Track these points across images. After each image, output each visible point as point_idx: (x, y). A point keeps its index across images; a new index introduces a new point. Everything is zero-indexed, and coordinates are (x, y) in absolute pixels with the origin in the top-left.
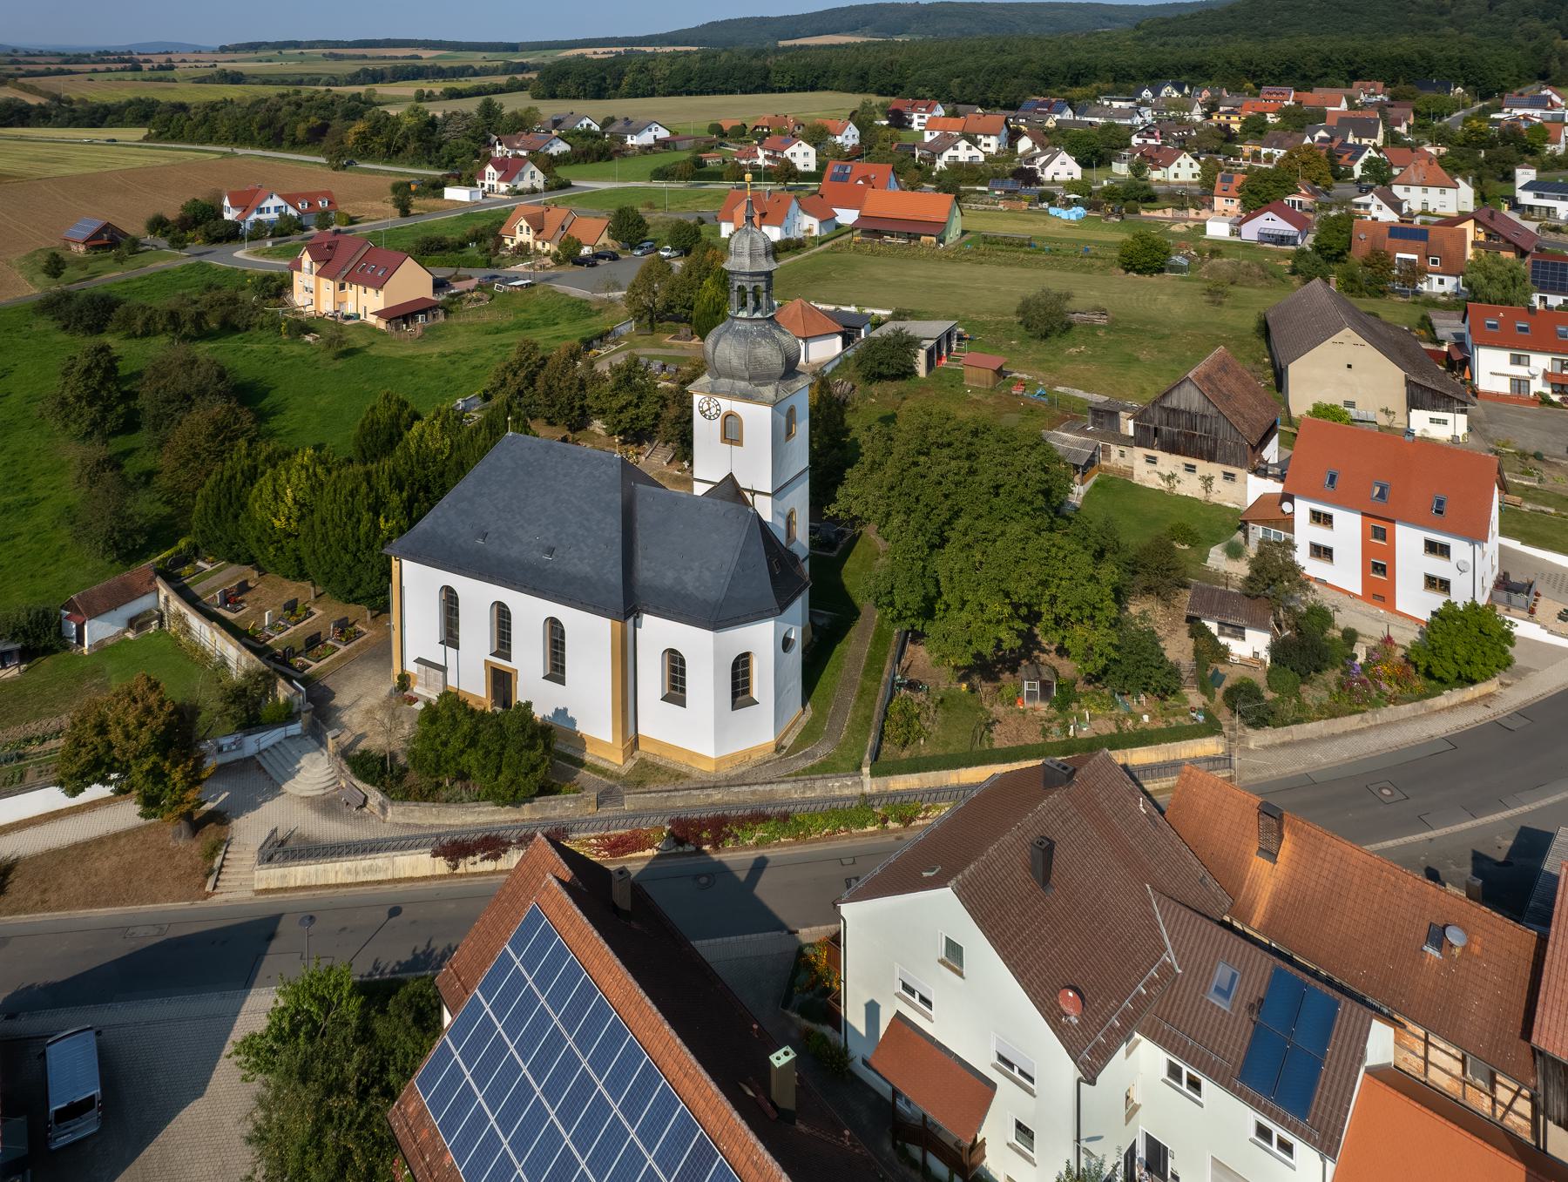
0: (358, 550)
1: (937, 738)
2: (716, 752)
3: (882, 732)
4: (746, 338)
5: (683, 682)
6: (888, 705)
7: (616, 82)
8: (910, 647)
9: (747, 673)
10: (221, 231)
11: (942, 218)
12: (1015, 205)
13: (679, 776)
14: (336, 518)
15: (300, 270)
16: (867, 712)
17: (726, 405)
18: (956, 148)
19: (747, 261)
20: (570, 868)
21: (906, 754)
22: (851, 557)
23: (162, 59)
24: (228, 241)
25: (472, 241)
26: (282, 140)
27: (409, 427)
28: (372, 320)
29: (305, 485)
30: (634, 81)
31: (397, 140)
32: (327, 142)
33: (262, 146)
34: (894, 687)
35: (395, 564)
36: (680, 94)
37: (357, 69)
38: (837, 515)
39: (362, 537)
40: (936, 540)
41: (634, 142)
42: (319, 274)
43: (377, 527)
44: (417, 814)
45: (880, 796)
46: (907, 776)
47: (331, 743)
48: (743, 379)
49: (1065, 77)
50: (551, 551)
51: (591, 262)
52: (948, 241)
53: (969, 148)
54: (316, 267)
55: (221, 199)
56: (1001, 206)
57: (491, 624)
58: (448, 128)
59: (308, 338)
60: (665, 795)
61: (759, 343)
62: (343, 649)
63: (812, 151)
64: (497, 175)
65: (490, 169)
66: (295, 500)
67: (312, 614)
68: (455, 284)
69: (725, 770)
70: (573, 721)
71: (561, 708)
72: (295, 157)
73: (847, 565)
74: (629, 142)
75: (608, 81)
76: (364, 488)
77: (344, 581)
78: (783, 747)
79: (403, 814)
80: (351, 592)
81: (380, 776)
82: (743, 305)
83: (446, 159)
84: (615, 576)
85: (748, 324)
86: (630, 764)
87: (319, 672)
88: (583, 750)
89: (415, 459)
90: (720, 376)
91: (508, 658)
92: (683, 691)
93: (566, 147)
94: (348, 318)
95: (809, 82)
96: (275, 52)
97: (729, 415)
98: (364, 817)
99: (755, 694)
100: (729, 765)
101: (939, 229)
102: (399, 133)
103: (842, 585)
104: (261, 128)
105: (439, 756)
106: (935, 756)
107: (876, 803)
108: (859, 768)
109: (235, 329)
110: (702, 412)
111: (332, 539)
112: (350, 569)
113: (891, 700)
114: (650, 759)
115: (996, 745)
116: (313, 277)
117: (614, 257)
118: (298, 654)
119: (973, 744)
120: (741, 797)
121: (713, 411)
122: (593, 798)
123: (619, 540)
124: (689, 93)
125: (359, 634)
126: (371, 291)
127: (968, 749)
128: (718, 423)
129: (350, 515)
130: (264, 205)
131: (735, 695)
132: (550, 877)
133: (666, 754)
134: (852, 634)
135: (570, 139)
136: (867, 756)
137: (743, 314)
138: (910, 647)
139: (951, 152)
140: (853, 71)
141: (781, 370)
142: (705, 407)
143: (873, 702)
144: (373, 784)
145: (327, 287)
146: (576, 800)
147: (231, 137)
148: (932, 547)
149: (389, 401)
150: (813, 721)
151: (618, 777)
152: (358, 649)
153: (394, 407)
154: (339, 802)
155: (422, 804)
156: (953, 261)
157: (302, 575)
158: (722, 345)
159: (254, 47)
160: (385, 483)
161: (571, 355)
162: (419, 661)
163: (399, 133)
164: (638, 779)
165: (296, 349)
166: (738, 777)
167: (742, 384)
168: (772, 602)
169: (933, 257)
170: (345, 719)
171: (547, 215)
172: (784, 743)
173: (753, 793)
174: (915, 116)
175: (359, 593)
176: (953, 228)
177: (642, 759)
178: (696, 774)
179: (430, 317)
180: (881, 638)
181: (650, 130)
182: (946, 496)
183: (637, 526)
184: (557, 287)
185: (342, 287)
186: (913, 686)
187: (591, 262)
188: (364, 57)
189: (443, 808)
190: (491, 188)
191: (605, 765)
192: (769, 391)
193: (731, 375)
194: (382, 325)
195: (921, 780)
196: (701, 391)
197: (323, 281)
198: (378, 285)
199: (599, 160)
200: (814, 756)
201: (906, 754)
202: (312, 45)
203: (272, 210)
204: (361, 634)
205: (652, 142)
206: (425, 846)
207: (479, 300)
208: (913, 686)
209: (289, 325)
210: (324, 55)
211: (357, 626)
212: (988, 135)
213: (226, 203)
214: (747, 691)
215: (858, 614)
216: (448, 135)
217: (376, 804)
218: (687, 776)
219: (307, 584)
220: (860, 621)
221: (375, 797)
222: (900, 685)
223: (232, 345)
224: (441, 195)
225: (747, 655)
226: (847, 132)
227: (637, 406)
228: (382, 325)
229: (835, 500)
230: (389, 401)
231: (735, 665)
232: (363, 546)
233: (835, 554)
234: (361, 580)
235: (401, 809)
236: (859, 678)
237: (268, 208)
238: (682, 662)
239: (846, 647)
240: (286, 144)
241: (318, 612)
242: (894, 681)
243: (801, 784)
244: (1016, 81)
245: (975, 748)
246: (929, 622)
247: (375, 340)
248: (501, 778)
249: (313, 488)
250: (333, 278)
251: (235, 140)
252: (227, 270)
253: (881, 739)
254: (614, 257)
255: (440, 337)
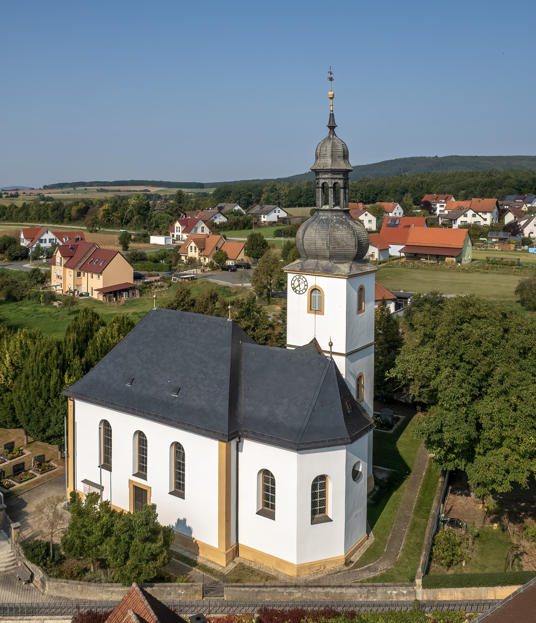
0: (49, 398)
1: (476, 562)
2: (299, 557)
3: (431, 554)
4: (328, 224)
5: (273, 499)
6: (435, 534)
7: (258, 198)
8: (450, 496)
9: (323, 494)
10: (18, 253)
11: (460, 245)
12: (506, 246)
13: (268, 577)
14: (35, 372)
15: (55, 265)
16: (418, 540)
17: (312, 280)
18: (466, 216)
19: (329, 161)
20: (156, 613)
21: (451, 572)
22: (404, 434)
23: (14, 193)
24: (22, 260)
25: (162, 259)
26: (64, 218)
27: (97, 330)
28: (96, 296)
29: (19, 352)
30: (268, 197)
31: (127, 215)
32: (89, 218)
33: (53, 222)
34: (439, 524)
35: (70, 403)
36: (295, 206)
37: (113, 196)
38: (396, 377)
39: (52, 389)
40: (476, 392)
41: (265, 220)
42: (65, 266)
43: (63, 382)
44: (67, 589)
45: (431, 604)
46: (452, 590)
47: (13, 533)
48: (324, 258)
49: (531, 188)
50: (178, 391)
51: (233, 269)
52: (463, 262)
53: (474, 216)
54: (64, 261)
55: (19, 235)
56: (496, 248)
57: (134, 450)
58: (156, 208)
59: (56, 304)
60: (256, 590)
61: (338, 228)
62: (39, 476)
63: (374, 219)
64: (182, 229)
65: (177, 224)
66: (12, 364)
67: (23, 454)
68: (148, 278)
69: (305, 576)
70: (190, 530)
71: (181, 518)
72: (70, 227)
73: (401, 439)
74: (263, 219)
75: (253, 197)
76: (55, 352)
77: (38, 421)
78: (352, 562)
79: (56, 588)
80: (44, 431)
81: (43, 558)
82: (326, 203)
83: (154, 225)
84: (223, 406)
85: (329, 214)
86: (232, 566)
87: (20, 490)
88: (197, 554)
89: (99, 350)
90: (307, 258)
91: (145, 477)
92: (273, 507)
93: (224, 220)
94: (82, 295)
95: (371, 197)
96: (72, 189)
97: (315, 289)
98: (30, 590)
99: (330, 513)
100: (307, 572)
101: (458, 253)
102: (128, 210)
103: (397, 452)
104: (53, 211)
105: (83, 543)
106: (475, 575)
107: (427, 609)
108: (413, 580)
109: (15, 300)
110: (294, 288)
111: (31, 387)
112: (43, 411)
113: (437, 531)
114: (247, 564)
115: (525, 569)
116: (62, 268)
117: (248, 267)
118: (8, 477)
119: (506, 569)
120: (317, 597)
121: (302, 286)
122: (200, 588)
123: (227, 381)
124: (300, 205)
125: (51, 468)
126: (95, 276)
127: (503, 571)
128: (305, 297)
129: (44, 370)
130: (43, 238)
131: (314, 512)
132: (130, 613)
133: (259, 560)
134: (405, 485)
135: (227, 216)
136: (420, 570)
137: (327, 207)
138: (450, 496)
139: (462, 218)
140: (399, 189)
141: (353, 250)
142: (296, 284)
143: (423, 533)
144: (38, 564)
145: (70, 273)
146: (186, 588)
147: (37, 218)
148: (474, 398)
149: (87, 313)
150: (375, 545)
151: (221, 575)
152: (49, 476)
153: (90, 317)
154: (15, 577)
155: (71, 581)
156: (467, 271)
157: (16, 423)
158: (309, 230)
159: (61, 186)
160: (70, 350)
161: (211, 297)
162: (86, 482)
163: (128, 210)
164: (237, 578)
165: (47, 309)
166: (314, 581)
167: (324, 263)
168: (346, 435)
169: (453, 269)
170: (30, 521)
171: (207, 240)
172: (352, 558)
173: (327, 594)
174: (438, 205)
175: (49, 432)
176: (467, 254)
177: (241, 564)
178: (281, 577)
179: (131, 294)
180: (428, 488)
181: (275, 212)
182: (485, 354)
183: (242, 373)
184: (211, 280)
185: (79, 275)
186: (454, 523)
187: (233, 269)
188: (119, 191)
189: (85, 585)
190: (178, 238)
191: (212, 566)
192: (345, 268)
193: (316, 256)
194: (101, 298)
195: (464, 594)
196: (293, 271)
197: (68, 270)
198: (99, 272)
199: (244, 228)
200: (376, 570)
201: (451, 572)
202: (91, 184)
203: (48, 241)
204: (54, 468)
205: (276, 220)
206: (69, 614)
207: (162, 287)
208: (454, 523)
209: (45, 296)
210: (98, 190)
211: (52, 463)
212: (485, 213)
213: (22, 236)
214: (323, 511)
215: (410, 471)
216: (156, 212)
217: (39, 580)
218: (274, 578)
219: (21, 432)
220: (411, 476)
221: (39, 574)
222: (444, 522)
223: (11, 308)
224: (148, 241)
225: (323, 478)
226: (395, 210)
227: (253, 329)
228: (101, 298)
229: (394, 366)
230: (87, 313)
231: (314, 487)
232: (52, 395)
233: (391, 432)
234: (50, 421)
235: (55, 584)
236: (412, 515)
237: (45, 240)
238: (273, 482)
239: (400, 493)
240: (66, 220)
241: (27, 452)
242: (439, 519)
243: (365, 590)
244: (500, 190)
245: (507, 571)
246: (469, 464)
247: (96, 306)
248: (129, 562)
249: (23, 355)
250: (73, 268)
251: (39, 219)
252: (17, 272)
253: (430, 560)
254: (248, 267)
255: (134, 305)
